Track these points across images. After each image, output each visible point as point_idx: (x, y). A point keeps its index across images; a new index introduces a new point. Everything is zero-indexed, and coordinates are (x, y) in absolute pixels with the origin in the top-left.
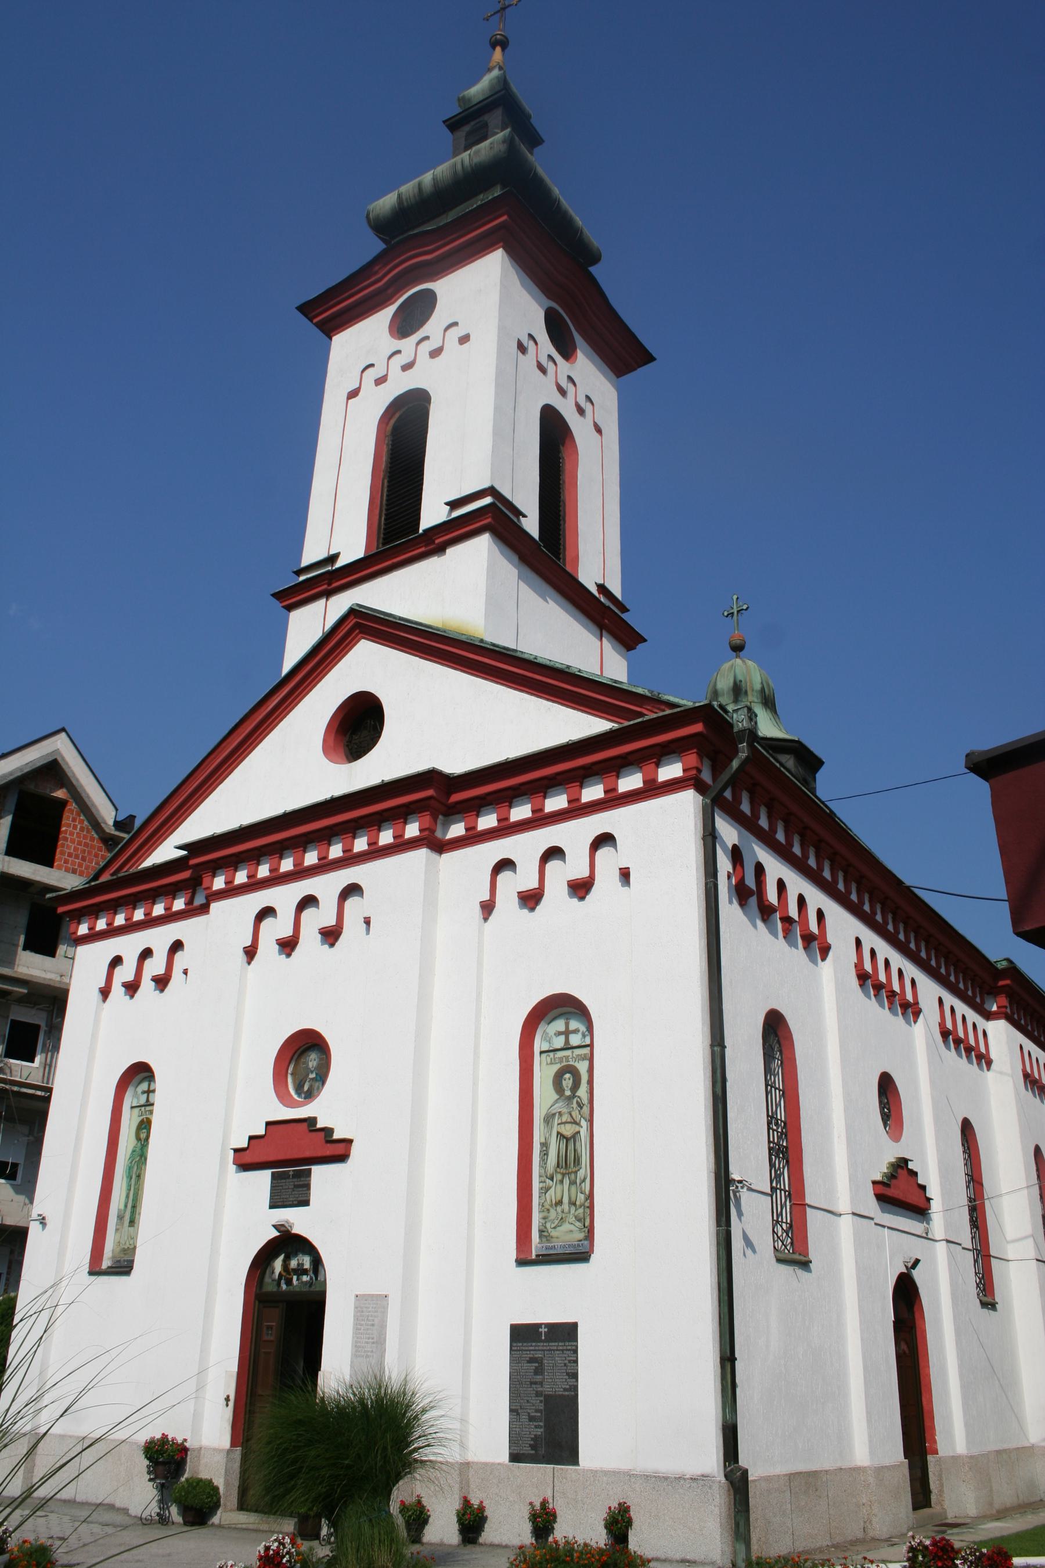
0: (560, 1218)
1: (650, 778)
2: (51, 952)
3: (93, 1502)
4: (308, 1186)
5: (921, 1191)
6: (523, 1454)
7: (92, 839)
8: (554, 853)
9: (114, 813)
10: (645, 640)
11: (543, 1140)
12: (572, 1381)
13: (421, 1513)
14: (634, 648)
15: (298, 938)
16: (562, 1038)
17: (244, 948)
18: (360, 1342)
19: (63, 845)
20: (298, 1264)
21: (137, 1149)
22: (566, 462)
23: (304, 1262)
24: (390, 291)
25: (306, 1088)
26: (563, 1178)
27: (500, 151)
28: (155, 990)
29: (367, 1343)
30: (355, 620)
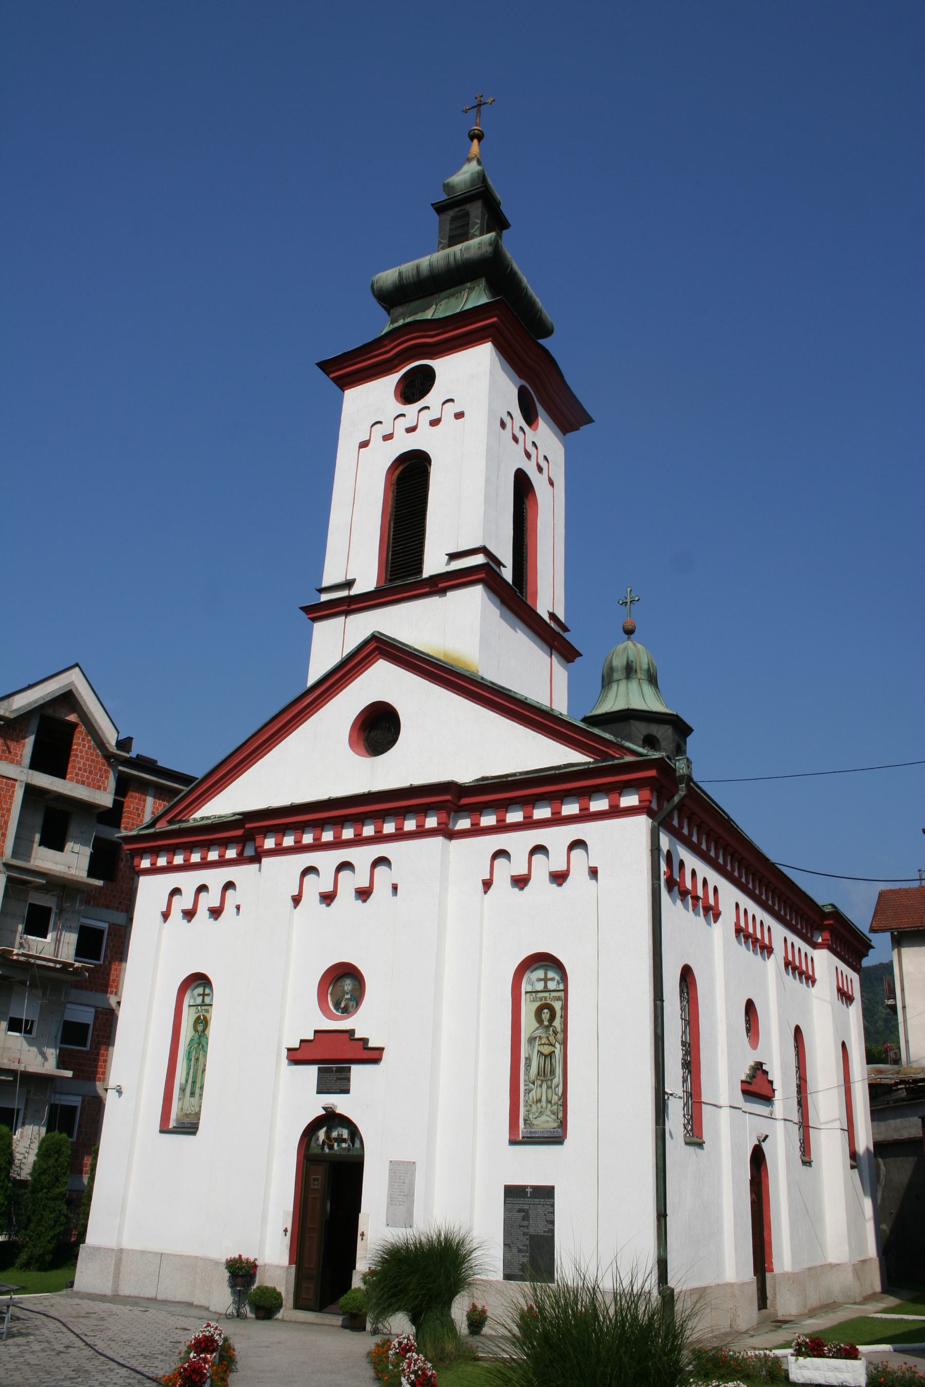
1: (613, 804)
2: (60, 847)
4: (348, 1079)
5: (769, 1085)
9: (116, 735)
10: (581, 655)
11: (527, 1056)
14: (573, 661)
15: (336, 893)
16: (542, 983)
17: (292, 896)
19: (74, 761)
20: (338, 1135)
22: (529, 511)
24: (396, 362)
25: (343, 1005)
27: (487, 251)
28: (209, 918)
29: (400, 1195)
30: (376, 644)
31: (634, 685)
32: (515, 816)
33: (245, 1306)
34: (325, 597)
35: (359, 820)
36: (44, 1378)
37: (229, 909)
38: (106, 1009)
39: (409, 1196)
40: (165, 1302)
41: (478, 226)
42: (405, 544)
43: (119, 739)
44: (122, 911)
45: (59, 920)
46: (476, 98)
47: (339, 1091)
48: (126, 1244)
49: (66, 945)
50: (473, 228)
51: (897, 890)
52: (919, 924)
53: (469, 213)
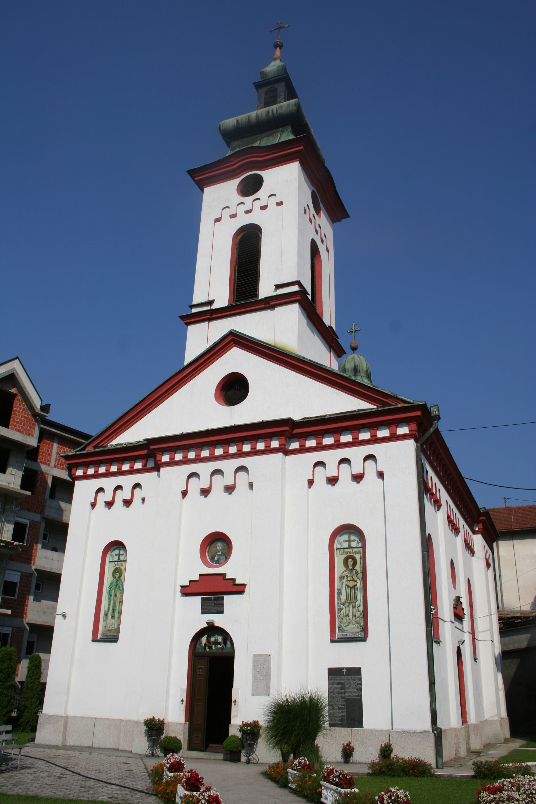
0: (348, 622)
3: (103, 747)
4: (222, 605)
6: (336, 723)
7: (28, 415)
9: (40, 402)
12: (359, 692)
15: (211, 489)
17: (182, 491)
18: (257, 675)
19: (14, 417)
20: (215, 640)
21: (114, 582)
23: (219, 639)
24: (238, 171)
25: (216, 559)
26: (349, 605)
27: (293, 110)
28: (123, 506)
29: (260, 676)
30: (232, 337)
32: (328, 441)
33: (157, 748)
34: (194, 310)
35: (226, 443)
36: (67, 792)
37: (137, 500)
38: (28, 573)
39: (267, 676)
40: (99, 749)
41: (283, 97)
42: (245, 280)
43: (42, 405)
44: (38, 513)
45: (3, 516)
46: (278, 24)
47: (216, 612)
48: (70, 713)
49: (6, 532)
50: (279, 98)
51: (493, 509)
52: (509, 528)
53: (277, 89)
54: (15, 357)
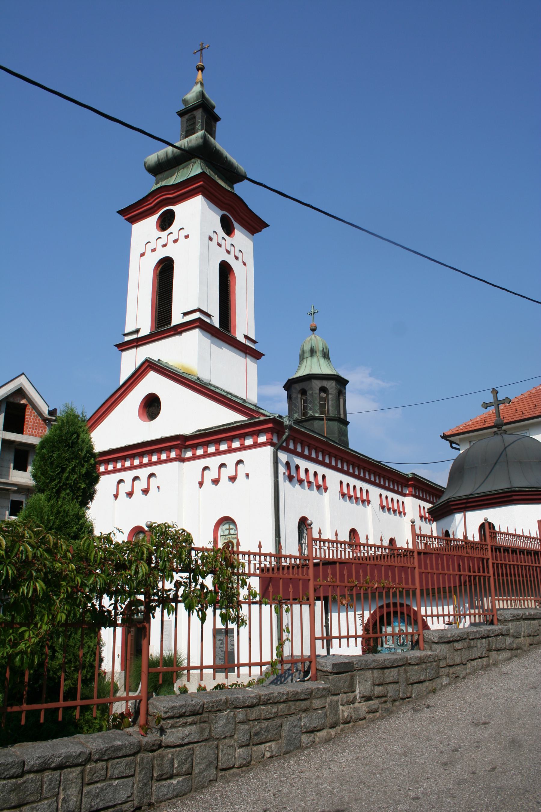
8: (223, 465)
9: (48, 408)
13: (186, 689)
19: (27, 424)
24: (156, 208)
31: (315, 359)
32: (211, 449)
34: (127, 339)
50: (197, 125)
54: (22, 373)
